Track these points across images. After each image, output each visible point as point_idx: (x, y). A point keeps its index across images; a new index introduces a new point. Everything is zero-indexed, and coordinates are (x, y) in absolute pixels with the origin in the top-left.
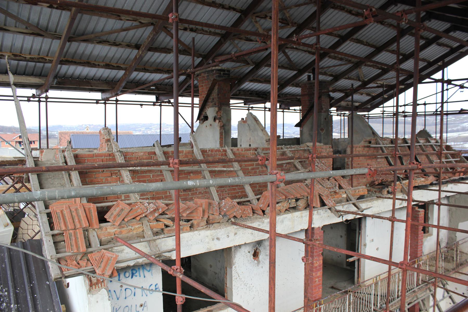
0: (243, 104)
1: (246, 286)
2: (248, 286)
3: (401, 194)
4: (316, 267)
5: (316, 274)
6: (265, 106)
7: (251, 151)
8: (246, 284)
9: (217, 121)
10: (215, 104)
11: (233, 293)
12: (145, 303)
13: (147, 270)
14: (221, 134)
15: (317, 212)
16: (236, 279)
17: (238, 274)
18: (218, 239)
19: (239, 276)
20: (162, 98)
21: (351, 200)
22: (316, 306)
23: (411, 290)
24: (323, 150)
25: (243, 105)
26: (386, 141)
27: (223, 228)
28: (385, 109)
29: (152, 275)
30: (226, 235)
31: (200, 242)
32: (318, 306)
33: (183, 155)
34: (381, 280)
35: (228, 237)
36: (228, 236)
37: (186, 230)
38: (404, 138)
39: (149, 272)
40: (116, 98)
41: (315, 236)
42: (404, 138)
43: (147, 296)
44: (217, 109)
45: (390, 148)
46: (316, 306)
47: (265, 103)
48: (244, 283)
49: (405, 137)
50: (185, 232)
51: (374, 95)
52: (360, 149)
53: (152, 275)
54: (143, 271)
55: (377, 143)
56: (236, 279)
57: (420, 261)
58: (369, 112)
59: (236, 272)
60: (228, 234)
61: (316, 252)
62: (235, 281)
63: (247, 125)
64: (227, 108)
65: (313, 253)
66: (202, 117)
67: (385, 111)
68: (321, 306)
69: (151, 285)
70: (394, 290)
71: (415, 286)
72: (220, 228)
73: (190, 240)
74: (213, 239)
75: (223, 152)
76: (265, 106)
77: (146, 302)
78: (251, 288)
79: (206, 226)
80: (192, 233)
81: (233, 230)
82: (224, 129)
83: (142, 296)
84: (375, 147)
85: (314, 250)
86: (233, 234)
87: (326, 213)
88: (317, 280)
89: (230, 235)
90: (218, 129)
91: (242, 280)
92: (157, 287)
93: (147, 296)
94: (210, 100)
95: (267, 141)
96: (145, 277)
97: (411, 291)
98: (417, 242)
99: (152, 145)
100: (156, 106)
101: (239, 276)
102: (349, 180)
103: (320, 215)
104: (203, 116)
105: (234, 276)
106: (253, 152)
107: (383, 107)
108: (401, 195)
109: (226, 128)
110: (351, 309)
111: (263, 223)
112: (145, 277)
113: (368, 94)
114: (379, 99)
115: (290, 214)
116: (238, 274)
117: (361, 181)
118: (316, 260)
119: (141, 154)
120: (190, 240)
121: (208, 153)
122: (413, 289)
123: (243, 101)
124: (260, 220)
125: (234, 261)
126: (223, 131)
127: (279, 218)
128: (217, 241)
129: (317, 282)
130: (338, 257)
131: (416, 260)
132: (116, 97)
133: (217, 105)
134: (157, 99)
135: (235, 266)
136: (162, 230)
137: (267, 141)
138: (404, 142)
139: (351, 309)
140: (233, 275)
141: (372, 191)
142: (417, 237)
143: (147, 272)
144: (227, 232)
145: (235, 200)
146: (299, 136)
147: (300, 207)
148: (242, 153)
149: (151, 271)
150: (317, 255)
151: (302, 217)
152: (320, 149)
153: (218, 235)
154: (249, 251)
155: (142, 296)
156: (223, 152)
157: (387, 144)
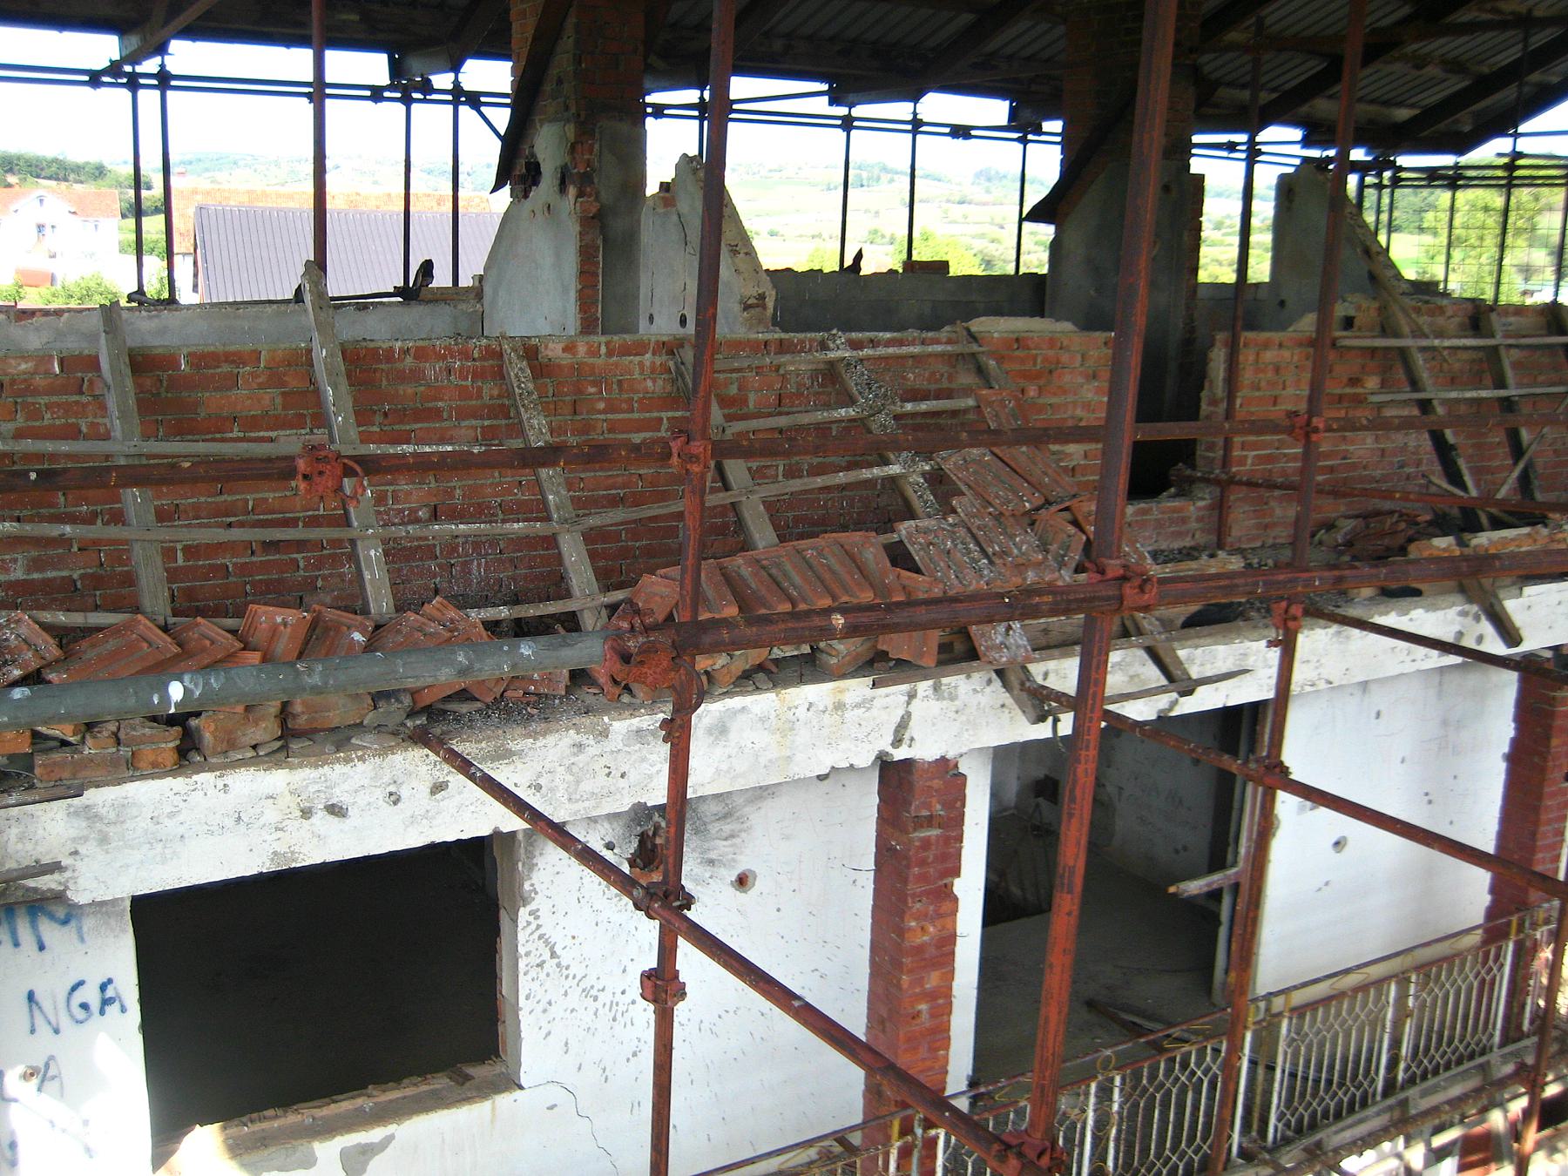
0: (826, 98)
1: (596, 999)
2: (604, 998)
3: (1459, 598)
4: (920, 949)
5: (920, 982)
6: (915, 114)
7: (648, 356)
8: (593, 992)
9: (572, 191)
10: (567, 108)
11: (523, 1026)
12: (47, 1066)
13: (52, 917)
14: (586, 255)
15: (936, 688)
16: (540, 965)
17: (547, 942)
18: (336, 810)
19: (553, 955)
20: (415, 64)
21: (1140, 632)
22: (906, 1130)
23: (1471, 1057)
24: (1065, 358)
25: (821, 105)
26: (1440, 320)
27: (361, 759)
28: (1524, 145)
29: (82, 939)
30: (380, 794)
31: (229, 822)
32: (919, 1131)
33: (254, 375)
34: (1293, 1010)
35: (395, 803)
36: (395, 799)
37: (155, 765)
38: (1555, 302)
39: (66, 929)
40: (162, 66)
41: (916, 803)
42: (1555, 302)
43: (57, 1031)
44: (570, 130)
45: (1465, 356)
46: (906, 1130)
47: (915, 98)
48: (585, 984)
49: (1560, 300)
50: (143, 777)
51: (1485, 70)
52: (1286, 354)
53: (82, 939)
54: (34, 925)
55: (1386, 328)
56: (540, 965)
57: (1534, 926)
58: (1461, 151)
59: (540, 937)
60: (392, 789)
61: (923, 878)
62: (533, 973)
63: (675, 218)
64: (624, 127)
65: (905, 881)
66: (520, 168)
67: (1520, 155)
68: (933, 1132)
69: (81, 983)
70: (1369, 1060)
71: (1497, 1038)
72: (348, 760)
73: (172, 815)
74: (306, 813)
75: (482, 358)
76: (915, 114)
77: (52, 1058)
78: (622, 1008)
79: (279, 744)
80: (180, 779)
81: (424, 769)
82: (603, 230)
83: (33, 1031)
84: (1373, 351)
85: (908, 867)
86: (425, 788)
87: (988, 690)
88: (923, 1007)
89: (405, 792)
90: (573, 228)
91: (571, 972)
92: (110, 993)
93: (57, 1031)
94: (548, 87)
95: (747, 307)
96: (42, 948)
97: (1467, 1065)
98: (1533, 835)
99: (290, 295)
100: (385, 104)
101: (553, 955)
102: (1211, 508)
103: (952, 698)
104: (523, 162)
105: (528, 954)
106: (658, 360)
107: (1516, 135)
108: (1454, 605)
109: (618, 225)
110: (1112, 1145)
111: (605, 733)
112: (42, 948)
113: (1455, 66)
114: (1508, 94)
115: (771, 696)
116: (547, 942)
117: (1278, 512)
118: (922, 916)
119: (23, 366)
120: (172, 815)
121: (399, 365)
122: (1483, 1053)
123: (825, 87)
124: (587, 721)
125: (527, 886)
126: (600, 242)
127: (707, 715)
128: (331, 818)
129: (925, 1016)
130: (1177, 852)
131: (1514, 919)
132: (158, 60)
133: (573, 110)
134: (396, 69)
135: (532, 906)
136: (27, 762)
137: (747, 307)
138: (1549, 325)
139: (1112, 1145)
140: (522, 950)
141: (650, 777)
142: (1536, 810)
143: (55, 926)
144: (386, 779)
145: (473, 613)
146: (1044, 270)
147: (834, 661)
148: (592, 367)
149: (73, 923)
150: (927, 893)
151: (839, 706)
152: (1051, 353)
153: (337, 791)
154: (608, 839)
155: (33, 1031)
156: (482, 358)
157: (1440, 334)
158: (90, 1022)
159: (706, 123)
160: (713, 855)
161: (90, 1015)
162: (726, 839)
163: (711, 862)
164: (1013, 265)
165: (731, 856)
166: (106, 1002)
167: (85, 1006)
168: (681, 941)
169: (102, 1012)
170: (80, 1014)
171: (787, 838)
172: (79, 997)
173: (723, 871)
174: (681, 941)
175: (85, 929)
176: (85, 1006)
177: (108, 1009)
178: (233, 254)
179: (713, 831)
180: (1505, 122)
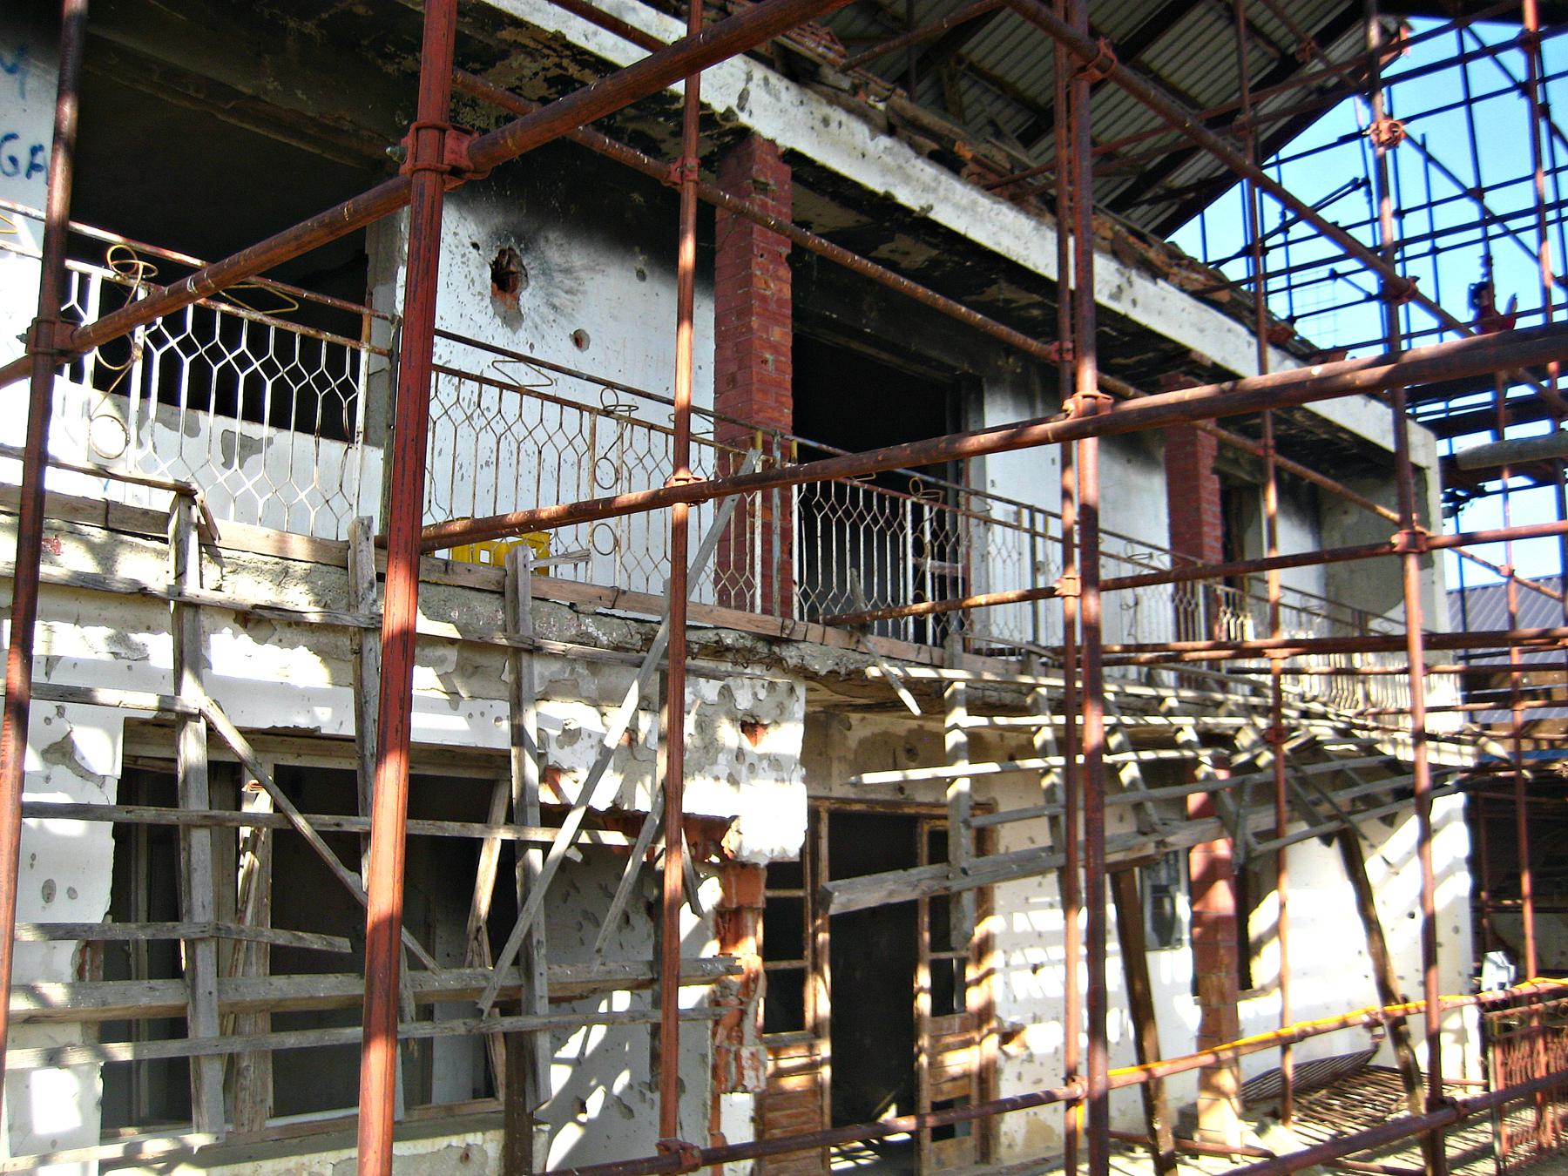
29: (23, 95)
39: (10, 78)
154: (475, 240)
158: (16, 178)
159: (1071, 241)
160: (557, 302)
161: (17, 172)
162: (566, 292)
163: (554, 307)
164: (1110, 529)
165: (570, 311)
166: (34, 167)
167: (13, 160)
168: (648, 54)
169: (28, 175)
170: (8, 167)
171: (614, 317)
172: (10, 148)
173: (563, 321)
174: (648, 54)
175: (28, 87)
176: (13, 160)
177: (35, 174)
178: (1007, 45)
179: (557, 280)
180: (1276, 152)
